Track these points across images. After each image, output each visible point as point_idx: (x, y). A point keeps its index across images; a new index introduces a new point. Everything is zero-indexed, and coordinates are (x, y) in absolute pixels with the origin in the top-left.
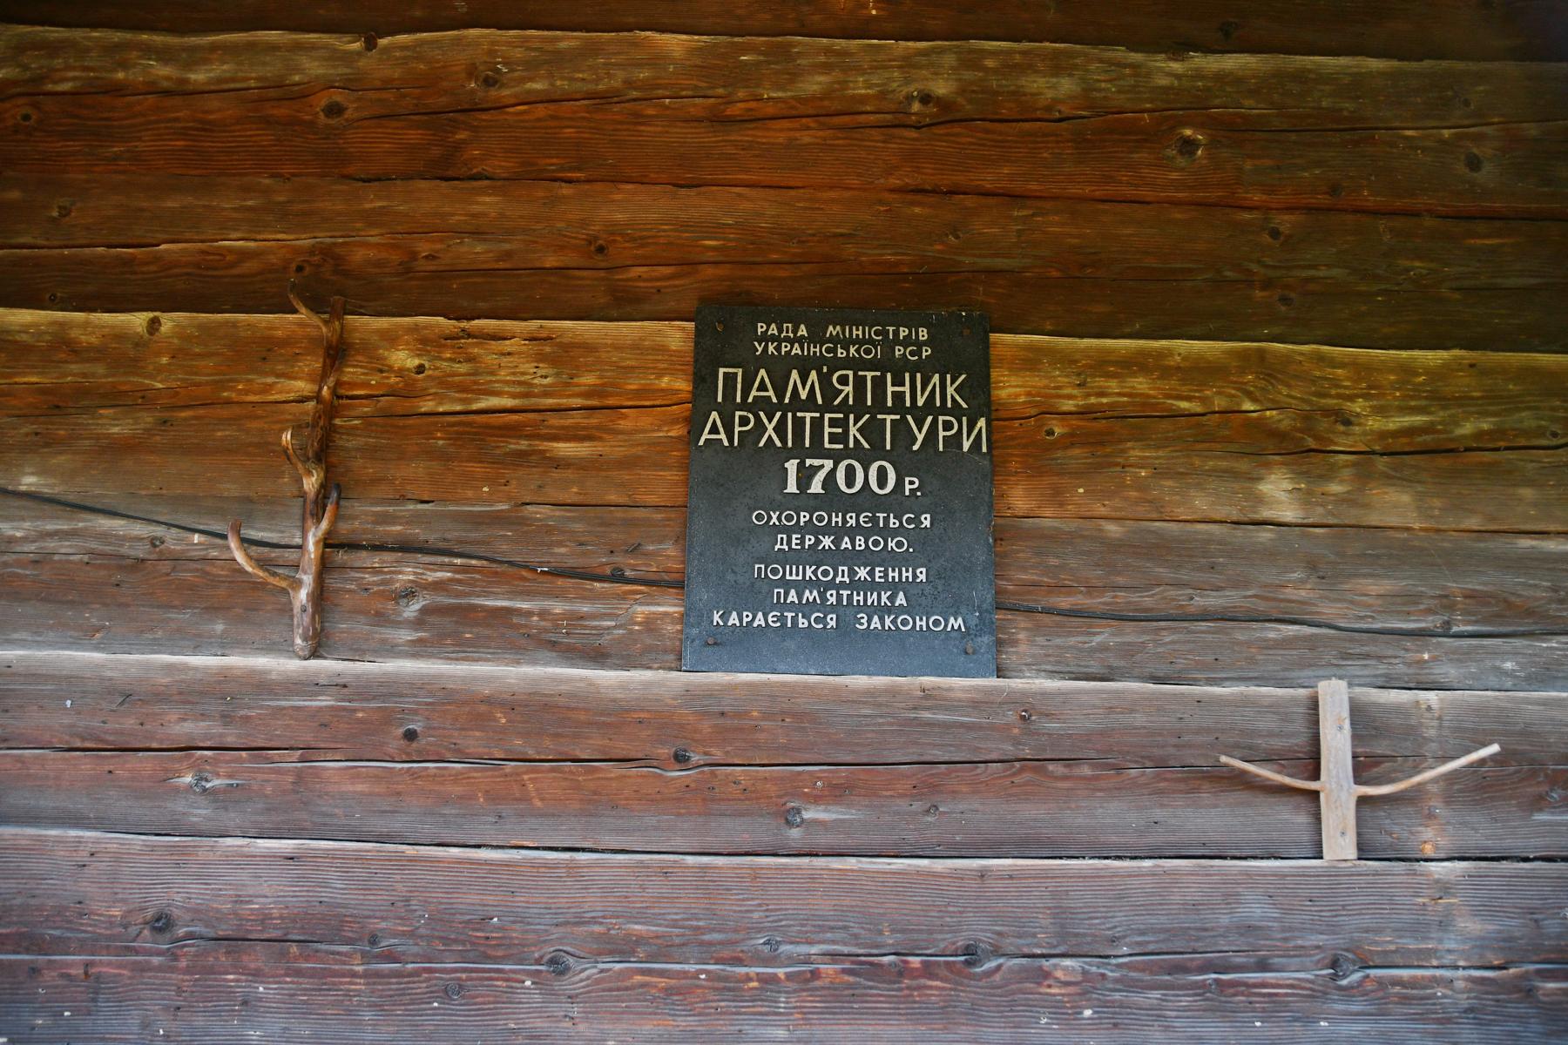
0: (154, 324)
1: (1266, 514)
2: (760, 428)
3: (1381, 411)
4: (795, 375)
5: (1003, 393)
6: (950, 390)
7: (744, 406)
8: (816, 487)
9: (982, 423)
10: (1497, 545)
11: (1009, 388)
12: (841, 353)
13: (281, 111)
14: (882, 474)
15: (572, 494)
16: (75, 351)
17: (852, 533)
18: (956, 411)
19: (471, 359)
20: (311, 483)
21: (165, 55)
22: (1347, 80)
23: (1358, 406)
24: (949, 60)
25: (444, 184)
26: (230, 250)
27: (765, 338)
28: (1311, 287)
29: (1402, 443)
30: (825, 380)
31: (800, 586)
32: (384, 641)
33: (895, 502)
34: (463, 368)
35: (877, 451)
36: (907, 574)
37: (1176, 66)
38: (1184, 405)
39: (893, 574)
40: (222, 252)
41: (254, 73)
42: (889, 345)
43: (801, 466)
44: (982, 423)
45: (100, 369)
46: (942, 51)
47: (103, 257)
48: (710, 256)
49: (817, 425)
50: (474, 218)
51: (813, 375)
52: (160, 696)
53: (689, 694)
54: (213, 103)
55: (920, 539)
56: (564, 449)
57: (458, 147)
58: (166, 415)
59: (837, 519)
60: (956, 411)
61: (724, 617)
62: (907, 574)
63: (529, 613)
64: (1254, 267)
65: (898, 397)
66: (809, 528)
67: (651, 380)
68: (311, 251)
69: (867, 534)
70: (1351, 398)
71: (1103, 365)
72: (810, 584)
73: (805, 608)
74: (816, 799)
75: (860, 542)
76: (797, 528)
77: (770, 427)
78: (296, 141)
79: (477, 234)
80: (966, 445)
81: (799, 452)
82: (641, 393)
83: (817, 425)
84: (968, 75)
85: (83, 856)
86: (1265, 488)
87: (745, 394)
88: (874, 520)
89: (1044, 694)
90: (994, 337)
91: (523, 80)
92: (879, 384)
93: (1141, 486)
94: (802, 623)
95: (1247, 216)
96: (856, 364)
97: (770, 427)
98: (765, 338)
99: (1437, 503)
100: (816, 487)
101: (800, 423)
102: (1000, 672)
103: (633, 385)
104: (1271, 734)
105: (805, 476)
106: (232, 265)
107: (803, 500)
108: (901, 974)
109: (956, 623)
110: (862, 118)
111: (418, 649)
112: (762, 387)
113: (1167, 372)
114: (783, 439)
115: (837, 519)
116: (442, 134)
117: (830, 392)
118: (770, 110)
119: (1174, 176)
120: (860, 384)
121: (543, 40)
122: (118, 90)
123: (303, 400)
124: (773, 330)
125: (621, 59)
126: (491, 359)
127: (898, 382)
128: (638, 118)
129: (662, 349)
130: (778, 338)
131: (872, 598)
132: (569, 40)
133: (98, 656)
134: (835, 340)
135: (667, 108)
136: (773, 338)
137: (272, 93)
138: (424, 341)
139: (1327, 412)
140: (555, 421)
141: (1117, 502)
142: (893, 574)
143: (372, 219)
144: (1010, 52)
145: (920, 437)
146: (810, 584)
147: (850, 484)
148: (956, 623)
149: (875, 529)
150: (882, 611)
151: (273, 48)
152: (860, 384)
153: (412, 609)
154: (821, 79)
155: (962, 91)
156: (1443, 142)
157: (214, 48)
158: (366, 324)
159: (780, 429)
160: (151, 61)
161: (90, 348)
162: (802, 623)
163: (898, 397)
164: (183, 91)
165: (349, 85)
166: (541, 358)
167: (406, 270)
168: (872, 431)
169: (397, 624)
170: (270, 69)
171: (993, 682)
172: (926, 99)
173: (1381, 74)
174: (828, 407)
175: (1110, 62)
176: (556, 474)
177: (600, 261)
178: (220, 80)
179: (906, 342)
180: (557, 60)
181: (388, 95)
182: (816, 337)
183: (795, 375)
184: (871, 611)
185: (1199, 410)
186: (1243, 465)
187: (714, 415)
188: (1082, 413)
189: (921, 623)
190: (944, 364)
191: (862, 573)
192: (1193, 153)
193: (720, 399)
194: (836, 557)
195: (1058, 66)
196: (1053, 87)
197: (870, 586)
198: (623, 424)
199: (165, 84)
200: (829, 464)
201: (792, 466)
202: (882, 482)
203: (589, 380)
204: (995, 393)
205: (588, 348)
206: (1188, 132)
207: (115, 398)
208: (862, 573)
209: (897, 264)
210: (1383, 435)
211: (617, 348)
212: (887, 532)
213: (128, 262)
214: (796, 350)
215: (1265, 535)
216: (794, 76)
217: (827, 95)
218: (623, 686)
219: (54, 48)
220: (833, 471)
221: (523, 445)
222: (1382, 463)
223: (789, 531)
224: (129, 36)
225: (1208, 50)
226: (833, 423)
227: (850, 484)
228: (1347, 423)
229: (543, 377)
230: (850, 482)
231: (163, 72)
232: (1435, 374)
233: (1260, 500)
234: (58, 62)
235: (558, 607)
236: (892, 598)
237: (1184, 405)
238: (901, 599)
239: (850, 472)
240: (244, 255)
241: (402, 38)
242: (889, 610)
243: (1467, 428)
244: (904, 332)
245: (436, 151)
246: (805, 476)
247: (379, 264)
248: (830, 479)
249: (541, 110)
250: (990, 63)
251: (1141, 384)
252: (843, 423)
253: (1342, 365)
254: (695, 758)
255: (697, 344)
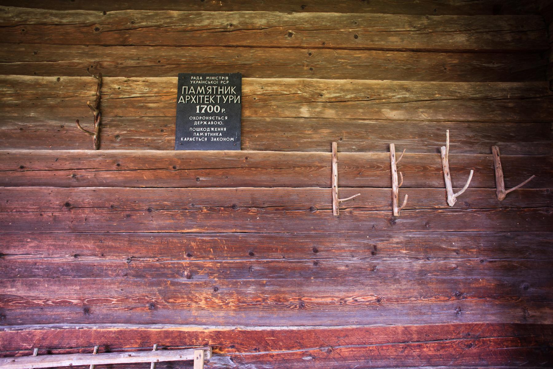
0: (59, 79)
1: (302, 115)
2: (191, 99)
3: (329, 93)
4: (199, 88)
5: (245, 91)
6: (232, 90)
7: (188, 94)
8: (203, 111)
9: (239, 97)
10: (354, 122)
11: (246, 89)
12: (209, 83)
13: (85, 30)
14: (217, 108)
15: (152, 115)
16: (41, 85)
17: (211, 121)
18: (233, 94)
19: (130, 86)
20: (95, 113)
21: (56, 15)
22: (329, 18)
23: (324, 92)
24: (237, 16)
25: (124, 47)
26: (76, 63)
27: (193, 80)
28: (318, 66)
29: (333, 100)
30: (205, 88)
31: (199, 132)
32: (113, 146)
33: (220, 114)
34: (128, 88)
35: (216, 103)
36: (222, 129)
37: (289, 16)
38: (285, 92)
39: (219, 129)
40: (73, 63)
41: (78, 20)
42: (220, 81)
43: (200, 107)
44: (239, 97)
45: (47, 89)
46: (236, 14)
47: (45, 64)
48: (183, 63)
49: (203, 98)
50: (129, 54)
51: (203, 88)
52: (65, 159)
53: (176, 155)
54: (68, 27)
55: (224, 121)
56: (151, 105)
57: (126, 38)
58: (63, 99)
59: (207, 118)
60: (233, 94)
61: (184, 139)
62: (222, 129)
63: (143, 140)
64: (305, 62)
65: (221, 92)
66: (202, 120)
67: (169, 90)
68: (94, 62)
69: (214, 121)
70: (323, 90)
71: (267, 84)
72: (202, 132)
73: (201, 137)
74: (202, 176)
75: (212, 123)
76: (199, 120)
77: (193, 99)
78: (94, 38)
79: (132, 58)
80: (235, 102)
81: (199, 104)
82: (167, 92)
83: (203, 98)
84: (241, 19)
85: (50, 191)
86: (302, 110)
87: (188, 92)
88: (215, 118)
89: (251, 154)
90: (243, 79)
91: (140, 22)
92: (217, 89)
93: (274, 110)
94: (200, 140)
95: (304, 50)
96: (212, 85)
97: (193, 99)
98: (193, 80)
99: (340, 113)
100: (203, 111)
101: (199, 98)
102: (242, 149)
103: (165, 90)
104: (300, 162)
105: (201, 109)
106: (76, 66)
107: (200, 114)
108: (219, 211)
109: (232, 139)
110: (217, 30)
111: (120, 148)
112: (192, 90)
113: (281, 85)
114: (196, 101)
115: (207, 118)
116: (123, 35)
117: (206, 91)
118: (196, 28)
119: (287, 41)
120: (213, 89)
121: (145, 13)
122: (45, 24)
123: (93, 95)
124: (195, 78)
125: (163, 17)
126: (135, 86)
127: (221, 88)
128: (167, 31)
129: (172, 83)
130: (196, 80)
131: (214, 134)
132: (151, 13)
133: (50, 151)
134: (208, 80)
135: (173, 29)
136: (195, 80)
137: (82, 25)
138: (120, 82)
139: (316, 93)
140: (149, 99)
141: (269, 113)
142: (219, 129)
143: (108, 55)
144: (251, 13)
145: (225, 100)
146: (202, 132)
147: (210, 110)
148: (232, 139)
149: (215, 120)
150: (216, 137)
151: (82, 14)
152: (213, 89)
153: (118, 140)
154: (207, 21)
155: (239, 23)
156: (350, 32)
157: (68, 14)
158: (107, 79)
159: (196, 99)
160: (53, 17)
161: (44, 84)
162: (200, 140)
163: (221, 92)
164: (60, 24)
165: (101, 23)
166: (146, 85)
167: (116, 67)
168: (215, 99)
169: (116, 142)
170: (81, 19)
171: (240, 151)
172: (231, 25)
173: (338, 17)
174: (206, 94)
175: (274, 15)
176: (149, 110)
177: (159, 64)
178: (70, 22)
179: (223, 80)
180: (149, 17)
181: (110, 26)
182: (204, 79)
183: (199, 88)
184: (214, 137)
185: (288, 93)
186: (297, 105)
187: (182, 97)
188: (263, 94)
189: (225, 139)
190: (231, 84)
191: (212, 129)
192: (291, 36)
193: (407, 196)
194: (207, 126)
195: (262, 17)
196: (261, 21)
197: (214, 132)
198: (163, 99)
199: (56, 23)
200: (206, 106)
201: (198, 107)
202: (217, 110)
203: (156, 90)
204: (243, 91)
205: (155, 83)
206: (290, 31)
207: (50, 96)
208: (212, 129)
209: (224, 63)
210: (329, 98)
211: (162, 83)
212: (218, 121)
213: (52, 65)
214: (200, 82)
215: (302, 120)
216: (202, 21)
217: (209, 25)
218: (162, 154)
219: (28, 13)
220: (207, 108)
221: (142, 104)
222: (329, 104)
223: (197, 121)
224: (46, 10)
225: (297, 11)
226: (207, 98)
227: (210, 110)
228: (322, 96)
229: (146, 90)
230: (210, 110)
231: (56, 20)
232: (343, 85)
233: (300, 113)
234: (30, 17)
235: (150, 138)
236: (219, 134)
237: (285, 92)
238: (221, 134)
239: (210, 108)
240: (79, 64)
241: (112, 12)
242: (218, 137)
243: (348, 97)
244: (223, 78)
245: (121, 39)
246: (201, 109)
247: (110, 65)
248: (206, 110)
249: (145, 29)
250: (246, 16)
251: (276, 88)
252: (209, 98)
253: (322, 83)
254: (177, 168)
255: (179, 82)
